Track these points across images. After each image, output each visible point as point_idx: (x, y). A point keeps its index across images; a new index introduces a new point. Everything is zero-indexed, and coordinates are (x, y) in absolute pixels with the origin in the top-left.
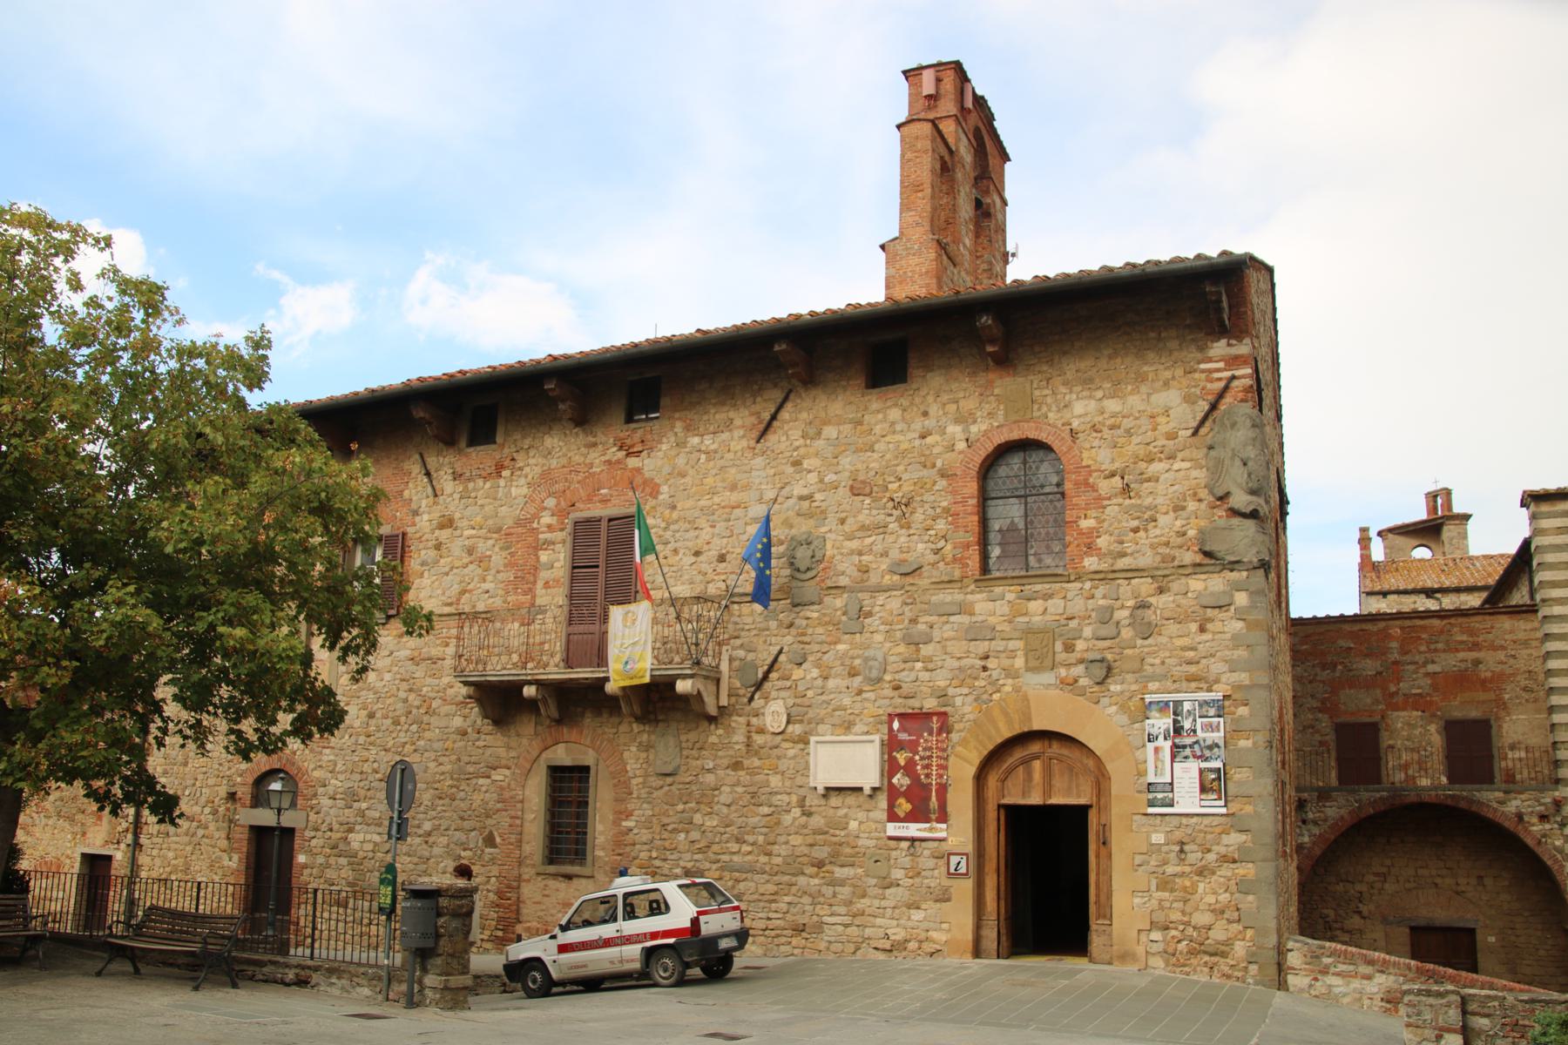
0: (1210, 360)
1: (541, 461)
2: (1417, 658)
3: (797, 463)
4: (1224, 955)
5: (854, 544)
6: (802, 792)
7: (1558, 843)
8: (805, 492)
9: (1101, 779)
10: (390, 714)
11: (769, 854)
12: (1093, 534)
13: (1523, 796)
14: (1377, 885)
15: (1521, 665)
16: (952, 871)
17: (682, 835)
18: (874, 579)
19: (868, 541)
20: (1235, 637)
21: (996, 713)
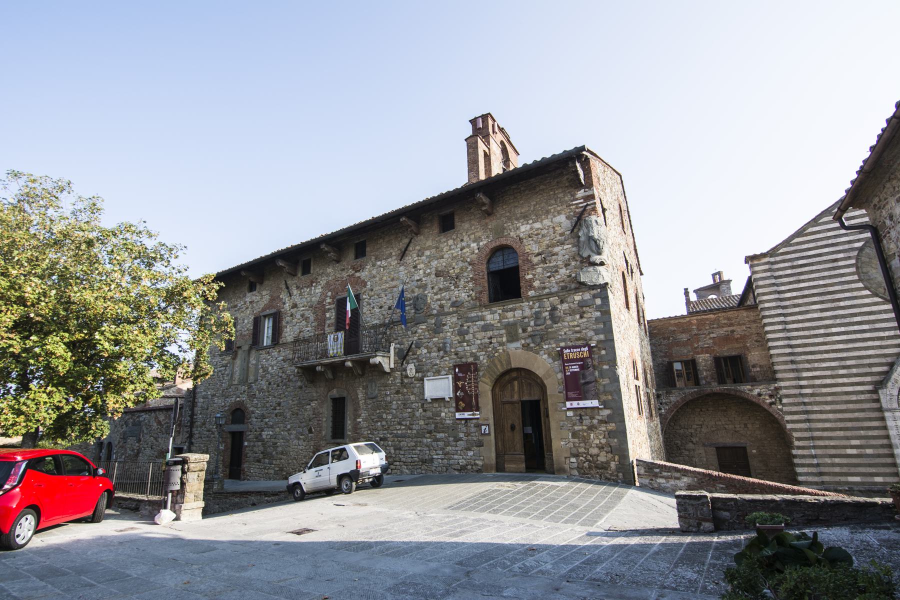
0: (577, 199)
1: (326, 278)
2: (705, 332)
3: (415, 267)
4: (606, 468)
5: (439, 296)
6: (423, 402)
7: (779, 407)
8: (418, 278)
9: (543, 387)
10: (276, 383)
11: (411, 429)
12: (531, 281)
13: (760, 387)
14: (699, 430)
15: (754, 331)
16: (483, 433)
17: (379, 423)
18: (446, 310)
19: (443, 295)
20: (596, 319)
21: (496, 361)
